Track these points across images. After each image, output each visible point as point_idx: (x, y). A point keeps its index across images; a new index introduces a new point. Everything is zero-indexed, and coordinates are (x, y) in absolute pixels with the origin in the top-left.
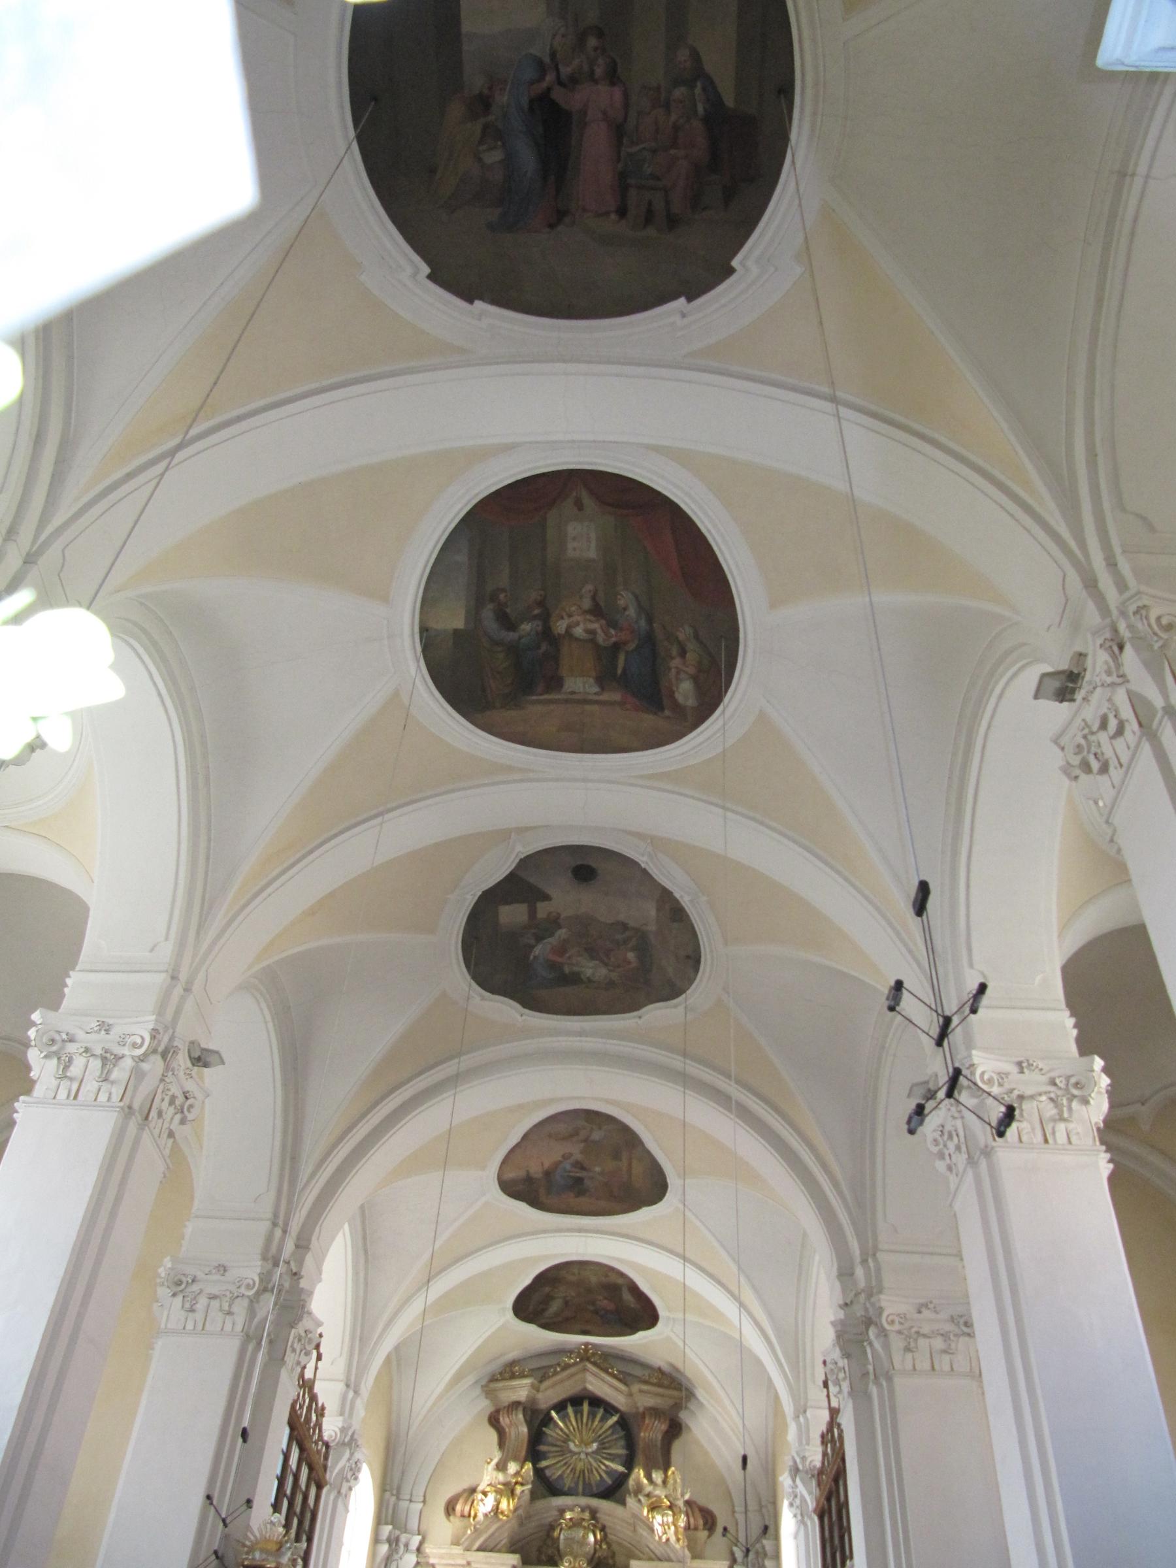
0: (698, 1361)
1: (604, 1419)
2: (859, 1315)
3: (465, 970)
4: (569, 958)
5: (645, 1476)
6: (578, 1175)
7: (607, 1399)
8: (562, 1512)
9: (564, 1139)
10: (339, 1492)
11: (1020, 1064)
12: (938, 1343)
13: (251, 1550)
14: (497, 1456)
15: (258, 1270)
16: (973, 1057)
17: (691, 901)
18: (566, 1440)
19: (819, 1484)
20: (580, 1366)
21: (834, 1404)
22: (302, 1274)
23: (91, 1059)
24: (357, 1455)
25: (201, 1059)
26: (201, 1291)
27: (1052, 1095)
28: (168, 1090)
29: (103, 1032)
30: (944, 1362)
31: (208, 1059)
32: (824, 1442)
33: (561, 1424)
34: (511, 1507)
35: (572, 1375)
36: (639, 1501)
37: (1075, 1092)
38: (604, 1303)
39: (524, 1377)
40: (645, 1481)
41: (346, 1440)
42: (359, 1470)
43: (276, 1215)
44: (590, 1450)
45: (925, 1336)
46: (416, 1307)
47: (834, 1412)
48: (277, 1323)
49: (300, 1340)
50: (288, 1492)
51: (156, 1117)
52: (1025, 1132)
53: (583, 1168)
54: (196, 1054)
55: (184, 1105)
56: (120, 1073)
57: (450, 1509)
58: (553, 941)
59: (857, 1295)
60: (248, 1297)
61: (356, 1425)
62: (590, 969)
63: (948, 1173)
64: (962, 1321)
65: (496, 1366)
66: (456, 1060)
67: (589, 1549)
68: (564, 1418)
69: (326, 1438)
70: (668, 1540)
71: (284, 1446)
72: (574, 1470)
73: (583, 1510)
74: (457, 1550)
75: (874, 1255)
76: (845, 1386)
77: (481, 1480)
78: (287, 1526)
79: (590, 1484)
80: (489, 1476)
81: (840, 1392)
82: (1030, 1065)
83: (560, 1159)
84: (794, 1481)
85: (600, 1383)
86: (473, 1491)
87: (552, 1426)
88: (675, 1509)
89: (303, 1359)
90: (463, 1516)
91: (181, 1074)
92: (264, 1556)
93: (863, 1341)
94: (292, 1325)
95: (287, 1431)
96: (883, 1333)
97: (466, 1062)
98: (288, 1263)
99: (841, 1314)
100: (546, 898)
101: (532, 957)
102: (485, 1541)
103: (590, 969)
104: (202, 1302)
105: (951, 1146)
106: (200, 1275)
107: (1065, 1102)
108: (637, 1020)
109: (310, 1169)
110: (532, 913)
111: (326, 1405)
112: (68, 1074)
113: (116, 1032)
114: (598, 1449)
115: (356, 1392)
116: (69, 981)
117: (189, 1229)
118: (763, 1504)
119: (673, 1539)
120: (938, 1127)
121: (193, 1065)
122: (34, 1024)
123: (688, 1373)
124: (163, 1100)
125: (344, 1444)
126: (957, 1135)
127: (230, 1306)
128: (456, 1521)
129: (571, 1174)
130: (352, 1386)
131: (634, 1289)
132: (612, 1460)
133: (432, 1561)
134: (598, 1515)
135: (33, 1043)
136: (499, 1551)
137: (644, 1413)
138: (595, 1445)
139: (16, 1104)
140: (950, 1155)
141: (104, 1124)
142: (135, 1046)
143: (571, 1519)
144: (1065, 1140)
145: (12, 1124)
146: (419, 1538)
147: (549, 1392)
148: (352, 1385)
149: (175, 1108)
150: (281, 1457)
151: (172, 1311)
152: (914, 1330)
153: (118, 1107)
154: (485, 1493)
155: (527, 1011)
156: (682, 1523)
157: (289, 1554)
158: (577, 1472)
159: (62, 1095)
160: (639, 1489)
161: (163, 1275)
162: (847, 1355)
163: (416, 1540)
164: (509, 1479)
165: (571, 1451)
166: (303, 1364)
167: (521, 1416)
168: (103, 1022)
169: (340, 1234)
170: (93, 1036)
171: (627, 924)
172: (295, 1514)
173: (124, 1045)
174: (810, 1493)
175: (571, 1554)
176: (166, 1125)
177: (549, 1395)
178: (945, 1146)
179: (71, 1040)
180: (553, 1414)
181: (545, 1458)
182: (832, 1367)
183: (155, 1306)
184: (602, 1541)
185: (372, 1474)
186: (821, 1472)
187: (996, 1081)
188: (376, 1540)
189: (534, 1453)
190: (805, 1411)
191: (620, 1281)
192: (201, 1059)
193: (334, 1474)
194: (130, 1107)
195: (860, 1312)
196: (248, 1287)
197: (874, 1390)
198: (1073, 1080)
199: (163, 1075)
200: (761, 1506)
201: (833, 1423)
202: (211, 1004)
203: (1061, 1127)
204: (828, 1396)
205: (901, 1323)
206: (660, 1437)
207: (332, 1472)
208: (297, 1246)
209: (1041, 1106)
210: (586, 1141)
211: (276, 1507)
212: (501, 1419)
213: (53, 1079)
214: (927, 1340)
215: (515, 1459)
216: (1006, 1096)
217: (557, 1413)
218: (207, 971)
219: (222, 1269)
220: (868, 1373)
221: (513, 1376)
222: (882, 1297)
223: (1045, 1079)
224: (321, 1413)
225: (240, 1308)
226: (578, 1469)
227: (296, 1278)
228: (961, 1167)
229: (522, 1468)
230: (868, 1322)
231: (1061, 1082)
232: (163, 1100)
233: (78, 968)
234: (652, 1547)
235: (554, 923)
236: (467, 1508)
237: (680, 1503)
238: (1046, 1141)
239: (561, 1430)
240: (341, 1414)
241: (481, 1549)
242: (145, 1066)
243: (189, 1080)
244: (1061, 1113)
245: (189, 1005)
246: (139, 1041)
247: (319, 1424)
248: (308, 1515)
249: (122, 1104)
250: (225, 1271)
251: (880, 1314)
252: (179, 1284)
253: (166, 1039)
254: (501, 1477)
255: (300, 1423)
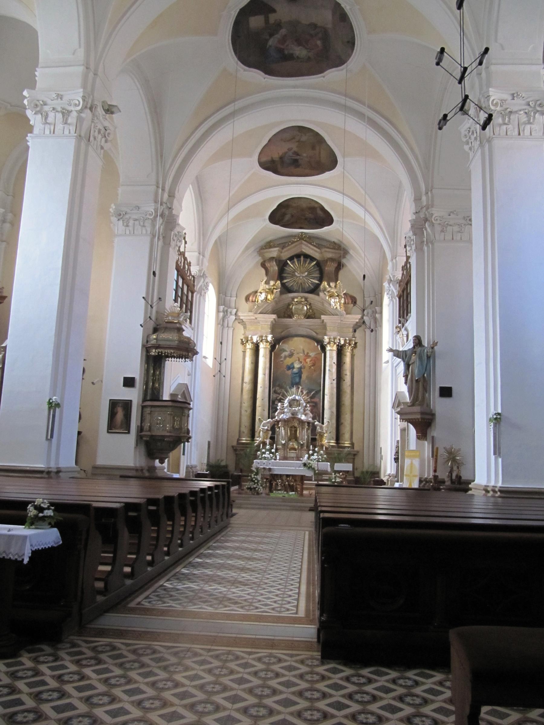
0: (349, 237)
1: (310, 263)
2: (422, 217)
3: (233, 53)
4: (287, 46)
5: (327, 285)
6: (296, 158)
7: (311, 255)
8: (293, 299)
9: (289, 140)
10: (201, 294)
11: (513, 95)
12: (456, 228)
13: (167, 316)
14: (265, 279)
15: (153, 207)
16: (490, 92)
17: (350, 9)
18: (294, 271)
19: (400, 286)
20: (300, 242)
21: (408, 255)
22: (173, 208)
23: (57, 113)
24: (207, 280)
25: (109, 110)
26: (130, 218)
27: (526, 111)
28: (97, 126)
29: (59, 99)
30: (458, 237)
31: (113, 110)
32: (403, 270)
33: (292, 266)
34: (272, 298)
35: (296, 246)
36: (325, 294)
37: (539, 109)
38: (309, 215)
39: (275, 247)
40: (327, 286)
41: (202, 275)
42: (208, 286)
43: (158, 183)
44: (304, 275)
45: (450, 225)
46: (224, 222)
47: (408, 258)
48: (165, 230)
49: (176, 236)
50: (180, 295)
51: (93, 140)
52: (509, 130)
53: (298, 155)
54: (107, 108)
55: (105, 133)
56: (72, 119)
57: (247, 299)
58: (278, 36)
59: (422, 208)
60: (151, 219)
61: (205, 269)
62: (299, 51)
63: (469, 151)
64: (468, 219)
65: (263, 243)
66: (233, 104)
67: (305, 312)
68: (293, 263)
69: (193, 274)
70: (336, 308)
71: (175, 278)
72: (298, 283)
73: (302, 298)
74: (251, 314)
75: (432, 190)
76: (414, 247)
77: (259, 288)
78: (181, 307)
79: (304, 288)
80: (262, 286)
81: (411, 250)
82: (518, 95)
83: (287, 151)
84: (389, 285)
85: (308, 248)
86: (256, 292)
87: (288, 266)
88: (340, 297)
89: (179, 244)
90: (252, 301)
91: (101, 118)
92: (173, 318)
93: (423, 228)
94: (172, 230)
95: (176, 272)
96: (433, 225)
97: (239, 104)
98: (166, 204)
99: (414, 217)
100: (274, 11)
101: (268, 46)
102: (262, 310)
103: (299, 51)
104: (131, 222)
105: (473, 137)
106: (128, 211)
107: (532, 114)
108: (322, 78)
109: (170, 161)
110: (267, 21)
111: (191, 262)
112: (48, 122)
113: (65, 98)
114: (308, 274)
115: (203, 256)
116: (36, 73)
117: (120, 190)
118: (377, 294)
119: (339, 307)
120: (468, 129)
121: (106, 113)
122: (25, 97)
123: (345, 242)
124: (95, 131)
125: (200, 276)
126: (476, 132)
127: (143, 223)
128: (250, 304)
129: (292, 158)
130: (201, 254)
131: (322, 209)
132: (314, 279)
133: (241, 318)
134: (308, 300)
135: (27, 107)
136: (268, 314)
137: (327, 260)
138: (306, 273)
139: (27, 138)
140: (471, 142)
141: (70, 145)
142: (76, 105)
143: (297, 301)
144: (529, 134)
145: (28, 148)
146: (236, 310)
147: (286, 253)
148: (201, 253)
149: (101, 135)
150: (175, 283)
151: (119, 226)
152: (446, 223)
153: (74, 136)
154: (261, 293)
155: (267, 76)
156: (343, 301)
157: (183, 317)
158: (299, 284)
159: (47, 132)
160: (325, 289)
161: (112, 212)
162: (415, 234)
163: (235, 310)
164: (270, 287)
165: (296, 276)
166: (179, 245)
167: (275, 263)
168: (58, 94)
169: (188, 191)
170: (55, 102)
171: (317, 24)
172: (184, 303)
173: (71, 105)
174: (396, 289)
175: (297, 314)
176: (99, 143)
177: (286, 255)
178: (470, 138)
179: (45, 104)
180: (289, 262)
181: (286, 279)
182: (408, 239)
183: (112, 225)
184: (309, 309)
185: (214, 287)
186: (401, 281)
187: (499, 104)
188: (218, 311)
189: (281, 276)
190: (396, 258)
191: (316, 205)
192: (109, 110)
193: (198, 288)
194: (80, 136)
195: (422, 215)
196: (150, 215)
197: (425, 248)
198: (538, 103)
199: (92, 119)
200: (375, 295)
201: (407, 262)
202: (109, 81)
203: (528, 127)
204: (406, 251)
205: (441, 220)
206: (334, 269)
207: (197, 287)
208: (169, 196)
209: (520, 116)
210: (298, 141)
211: (176, 301)
212: (266, 264)
213: (41, 125)
214: (451, 227)
215: (273, 280)
216: (503, 112)
217: (290, 261)
218: (103, 63)
219: (137, 208)
220: (423, 242)
221: (271, 247)
222: (433, 209)
223: (524, 102)
224: (189, 264)
225: (148, 224)
226: (299, 283)
227: (170, 210)
228: (476, 148)
229: (276, 283)
230: (426, 220)
231: (532, 104)
232: (95, 131)
233: (39, 66)
234: (330, 310)
235: (279, 25)
236: (254, 299)
237: (342, 294)
238: (519, 134)
239: (292, 267)
240: (198, 265)
241: (260, 313)
242: (83, 115)
243: (106, 121)
244: (529, 120)
245: (98, 81)
246: (77, 102)
247: (189, 269)
248: (189, 304)
249: (76, 135)
250: (139, 208)
251: (432, 216)
252: (120, 215)
253: (90, 101)
254: (267, 287)
255: (181, 269)
